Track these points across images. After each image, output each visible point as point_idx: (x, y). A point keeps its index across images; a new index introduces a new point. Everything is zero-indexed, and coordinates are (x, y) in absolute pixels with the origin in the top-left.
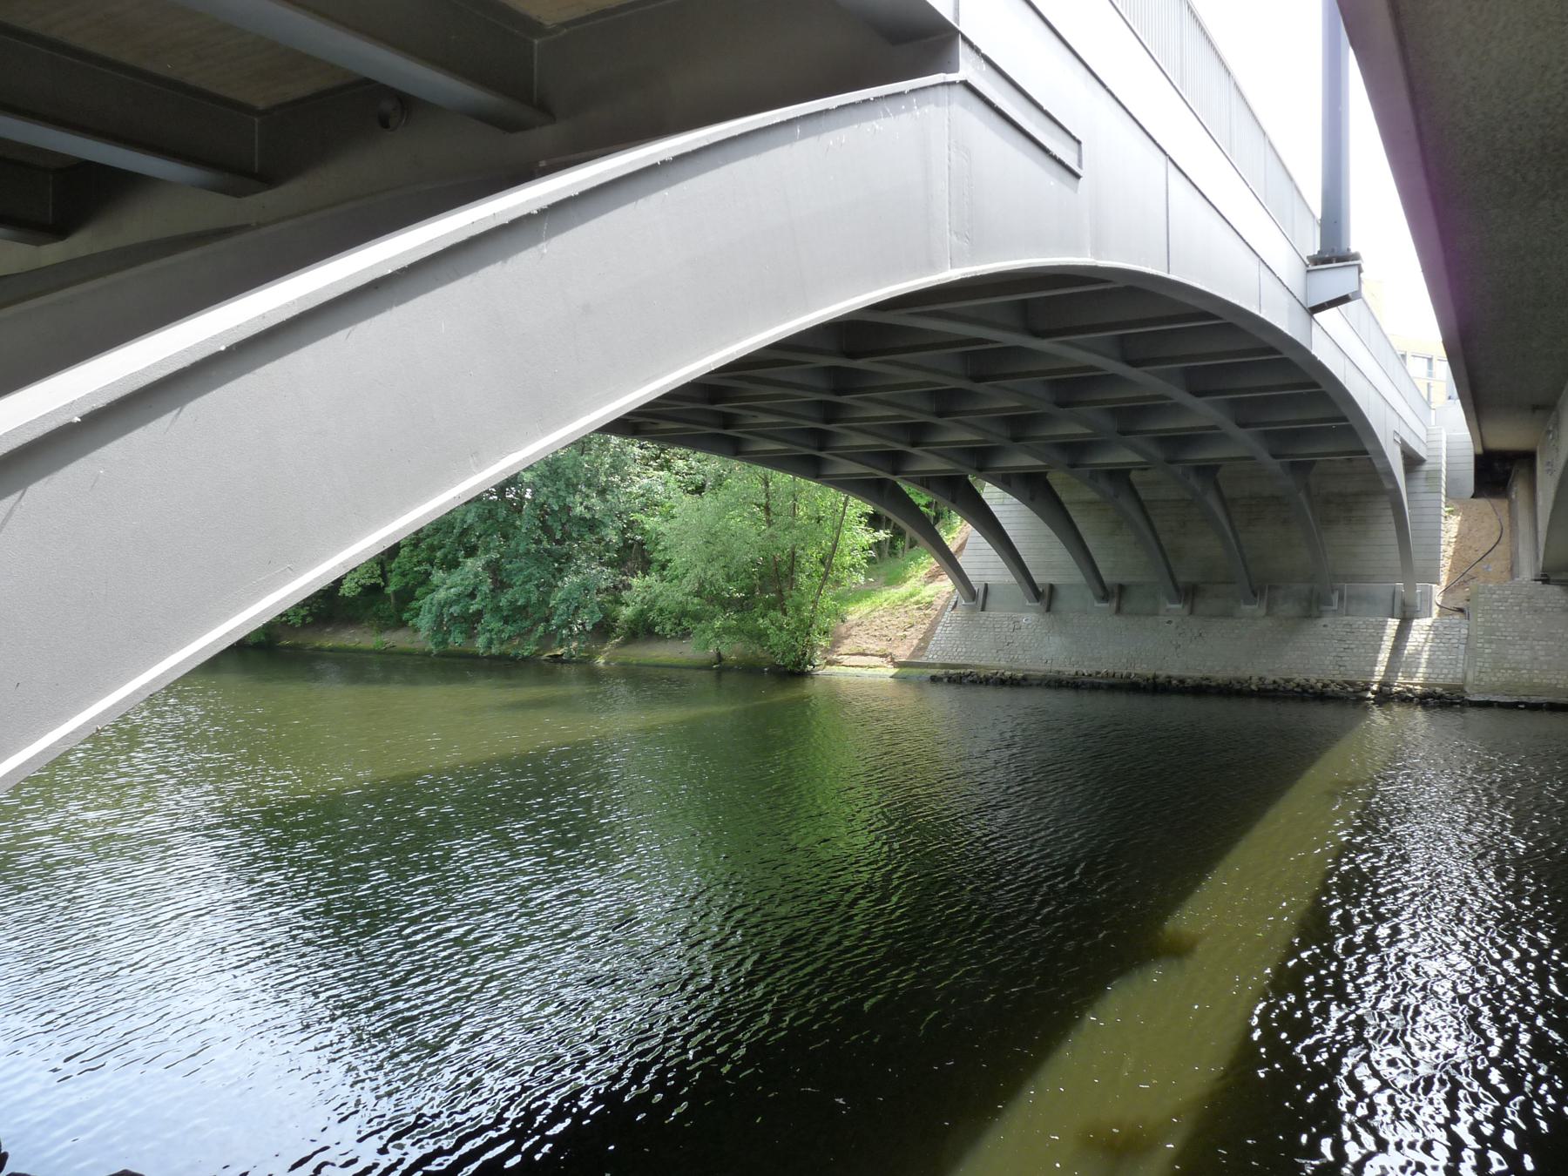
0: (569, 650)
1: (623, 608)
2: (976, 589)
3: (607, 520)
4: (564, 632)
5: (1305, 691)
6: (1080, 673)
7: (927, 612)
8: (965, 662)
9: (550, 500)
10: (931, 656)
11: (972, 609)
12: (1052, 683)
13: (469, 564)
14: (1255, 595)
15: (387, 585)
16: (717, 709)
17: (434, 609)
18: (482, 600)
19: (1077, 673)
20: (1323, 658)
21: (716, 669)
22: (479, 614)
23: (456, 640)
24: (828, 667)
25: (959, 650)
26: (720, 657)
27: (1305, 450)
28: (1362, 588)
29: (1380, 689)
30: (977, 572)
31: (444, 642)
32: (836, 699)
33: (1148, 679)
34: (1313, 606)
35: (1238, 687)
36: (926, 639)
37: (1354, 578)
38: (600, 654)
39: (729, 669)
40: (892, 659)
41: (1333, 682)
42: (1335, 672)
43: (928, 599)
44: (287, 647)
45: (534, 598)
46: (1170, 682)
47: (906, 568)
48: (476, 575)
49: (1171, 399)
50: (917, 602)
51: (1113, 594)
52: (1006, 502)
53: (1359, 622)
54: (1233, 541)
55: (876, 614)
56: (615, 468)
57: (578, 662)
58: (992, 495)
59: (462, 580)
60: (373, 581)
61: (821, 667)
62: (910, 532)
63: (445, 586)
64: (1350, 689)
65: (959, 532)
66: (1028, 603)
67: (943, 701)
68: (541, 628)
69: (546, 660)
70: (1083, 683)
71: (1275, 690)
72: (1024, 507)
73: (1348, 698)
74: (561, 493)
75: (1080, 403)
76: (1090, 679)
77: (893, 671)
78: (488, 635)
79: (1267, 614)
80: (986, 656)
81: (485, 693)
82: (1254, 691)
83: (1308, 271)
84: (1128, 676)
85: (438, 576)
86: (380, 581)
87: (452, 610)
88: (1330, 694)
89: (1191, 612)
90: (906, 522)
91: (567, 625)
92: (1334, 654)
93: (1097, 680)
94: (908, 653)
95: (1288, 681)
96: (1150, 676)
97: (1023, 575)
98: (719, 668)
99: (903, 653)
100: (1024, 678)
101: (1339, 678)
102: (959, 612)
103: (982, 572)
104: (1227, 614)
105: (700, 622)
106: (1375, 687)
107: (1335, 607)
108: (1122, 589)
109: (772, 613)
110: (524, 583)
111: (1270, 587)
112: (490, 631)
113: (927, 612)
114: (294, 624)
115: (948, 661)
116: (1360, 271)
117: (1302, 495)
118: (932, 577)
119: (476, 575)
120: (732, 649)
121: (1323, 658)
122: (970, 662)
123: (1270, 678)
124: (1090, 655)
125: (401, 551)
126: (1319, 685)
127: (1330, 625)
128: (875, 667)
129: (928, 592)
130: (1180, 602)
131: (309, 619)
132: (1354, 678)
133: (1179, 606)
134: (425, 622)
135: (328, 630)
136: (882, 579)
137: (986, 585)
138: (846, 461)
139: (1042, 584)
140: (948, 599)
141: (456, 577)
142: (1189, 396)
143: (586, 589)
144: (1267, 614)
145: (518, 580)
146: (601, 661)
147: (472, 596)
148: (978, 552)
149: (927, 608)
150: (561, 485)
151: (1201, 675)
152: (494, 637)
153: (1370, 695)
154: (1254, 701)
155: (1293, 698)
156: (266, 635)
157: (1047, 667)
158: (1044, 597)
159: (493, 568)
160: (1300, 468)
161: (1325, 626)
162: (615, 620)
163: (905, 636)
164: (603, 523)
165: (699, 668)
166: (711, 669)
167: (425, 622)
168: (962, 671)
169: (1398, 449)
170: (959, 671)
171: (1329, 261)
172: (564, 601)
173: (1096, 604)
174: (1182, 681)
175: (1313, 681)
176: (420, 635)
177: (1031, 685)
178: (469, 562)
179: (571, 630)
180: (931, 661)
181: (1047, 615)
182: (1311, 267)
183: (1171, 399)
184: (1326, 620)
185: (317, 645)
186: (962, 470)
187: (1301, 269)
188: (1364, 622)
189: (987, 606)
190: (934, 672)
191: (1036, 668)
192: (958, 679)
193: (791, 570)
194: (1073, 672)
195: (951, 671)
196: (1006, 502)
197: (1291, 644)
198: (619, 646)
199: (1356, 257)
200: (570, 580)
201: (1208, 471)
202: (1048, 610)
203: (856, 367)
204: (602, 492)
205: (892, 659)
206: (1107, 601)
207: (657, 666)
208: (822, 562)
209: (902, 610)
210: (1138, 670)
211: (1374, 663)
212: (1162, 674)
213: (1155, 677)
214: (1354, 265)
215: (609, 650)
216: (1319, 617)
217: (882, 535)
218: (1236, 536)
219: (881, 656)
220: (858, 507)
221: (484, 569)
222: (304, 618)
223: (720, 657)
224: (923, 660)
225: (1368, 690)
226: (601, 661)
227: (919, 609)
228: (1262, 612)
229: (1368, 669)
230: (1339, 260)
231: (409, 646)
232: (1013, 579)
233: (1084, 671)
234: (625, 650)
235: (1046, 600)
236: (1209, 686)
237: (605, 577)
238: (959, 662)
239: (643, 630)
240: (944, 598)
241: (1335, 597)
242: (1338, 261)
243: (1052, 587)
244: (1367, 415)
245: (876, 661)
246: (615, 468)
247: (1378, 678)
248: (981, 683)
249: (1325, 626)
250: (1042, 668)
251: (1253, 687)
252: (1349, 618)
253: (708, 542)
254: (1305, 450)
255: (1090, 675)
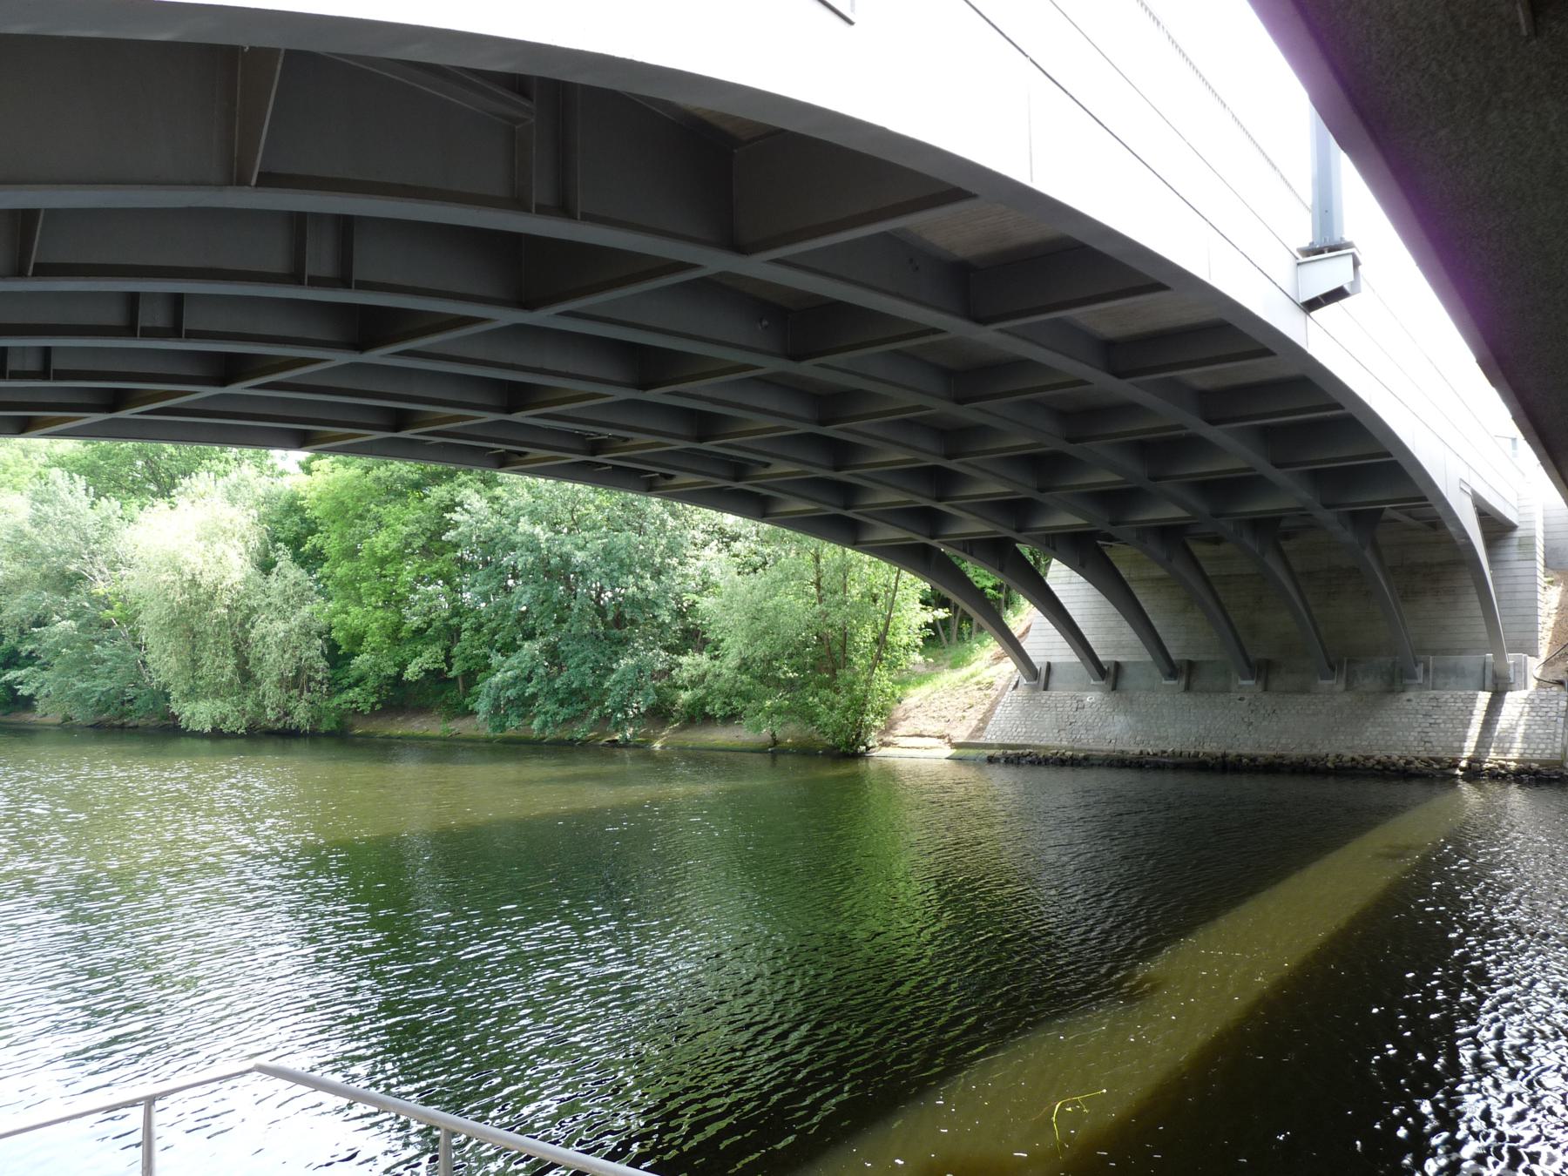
0: (625, 736)
1: (681, 692)
2: (1038, 668)
3: (661, 601)
4: (619, 715)
5: (1386, 768)
6: (1145, 752)
7: (987, 692)
8: (1025, 742)
9: (603, 580)
10: (991, 736)
11: (1034, 689)
12: (1115, 763)
13: (526, 646)
14: (1332, 668)
15: (450, 669)
16: (763, 781)
17: (492, 692)
18: (538, 683)
19: (1141, 752)
20: (1407, 734)
21: (772, 752)
22: (534, 696)
23: (513, 726)
24: (884, 749)
25: (1019, 730)
26: (775, 742)
27: (1364, 498)
28: (1453, 660)
29: (1469, 765)
30: (1043, 653)
31: (502, 727)
32: (889, 774)
33: (1217, 758)
34: (1397, 679)
35: (1313, 764)
36: (984, 720)
37: (1447, 651)
38: (657, 739)
39: (784, 751)
40: (950, 740)
41: (1417, 758)
42: (1420, 749)
43: (989, 680)
44: (359, 735)
45: (589, 682)
46: (1241, 760)
47: (971, 650)
48: (533, 658)
49: (1186, 428)
50: (978, 683)
51: (1182, 672)
52: (1073, 580)
53: (1446, 695)
54: (1305, 615)
55: (935, 695)
56: (672, 550)
57: (637, 746)
58: (1061, 577)
59: (519, 663)
60: (436, 666)
61: (877, 749)
62: (978, 618)
63: (503, 670)
64: (1436, 766)
65: (1025, 617)
66: (1092, 682)
67: (1003, 781)
68: (596, 712)
69: (603, 745)
70: (1147, 763)
71: (1353, 768)
72: (1090, 586)
73: (1434, 776)
74: (615, 574)
75: (1090, 439)
76: (1156, 759)
77: (951, 752)
78: (543, 717)
79: (1347, 690)
80: (1048, 736)
81: (537, 769)
82: (1330, 769)
83: (1299, 264)
84: (1196, 755)
85: (496, 659)
86: (444, 666)
87: (508, 693)
88: (1413, 771)
89: (1265, 689)
90: (971, 605)
91: (622, 708)
92: (1419, 729)
93: (1163, 760)
94: (966, 734)
95: (1367, 758)
96: (1219, 755)
97: (1083, 648)
98: (774, 751)
99: (961, 735)
100: (1086, 758)
101: (1424, 755)
102: (1021, 691)
103: (1049, 653)
104: (1304, 690)
105: (749, 702)
106: (1463, 764)
107: (1420, 681)
108: (1191, 665)
109: (823, 692)
110: (578, 666)
111: (1348, 662)
112: (546, 713)
113: (987, 692)
114: (363, 711)
115: (1007, 742)
116: (1356, 264)
117: (1368, 554)
118: (998, 659)
119: (533, 658)
120: (790, 732)
121: (1407, 734)
122: (1030, 742)
123: (1348, 755)
124: (1156, 734)
125: (462, 636)
126: (1402, 762)
127: (1414, 699)
128: (931, 748)
129: (987, 675)
130: (1253, 679)
131: (378, 707)
132: (1442, 755)
133: (1251, 682)
134: (483, 706)
135: (399, 719)
136: (948, 663)
137: (1049, 664)
138: (884, 525)
139: (1107, 662)
140: (1010, 679)
141: (513, 660)
142: (1203, 423)
143: (640, 670)
144: (1347, 690)
145: (573, 662)
146: (657, 745)
147: (529, 679)
148: (1044, 633)
149: (988, 688)
150: (615, 565)
151: (1273, 753)
152: (549, 719)
153: (1458, 772)
154: (1331, 779)
155: (1374, 776)
156: (338, 723)
157: (1111, 747)
158: (1109, 675)
159: (552, 653)
160: (1365, 520)
161: (1409, 700)
162: (673, 704)
163: (964, 717)
164: (657, 604)
165: (753, 751)
166: (768, 752)
167: (483, 706)
168: (1020, 752)
169: (1468, 503)
170: (1017, 751)
171: (1321, 251)
172: (617, 683)
173: (1164, 682)
174: (1253, 759)
175: (1395, 758)
176: (479, 725)
177: (1092, 765)
178: (526, 645)
179: (626, 714)
180: (989, 742)
181: (1113, 693)
182: (1302, 259)
183: (1186, 428)
184: (1411, 695)
185: (387, 733)
186: (1006, 532)
187: (1289, 262)
188: (1452, 697)
189: (1050, 686)
190: (991, 752)
191: (1100, 747)
192: (1016, 758)
193: (844, 648)
194: (1137, 751)
195: (1009, 752)
196: (1073, 580)
197: (1372, 720)
198: (676, 730)
199: (1349, 245)
200: (625, 662)
201: (1265, 527)
202: (1114, 688)
203: (948, 466)
204: (657, 574)
205: (950, 740)
206: (1175, 679)
207: (712, 749)
208: (877, 641)
209: (962, 691)
210: (1207, 749)
211: (1464, 739)
212: (1233, 752)
213: (1224, 756)
214: (1348, 254)
215: (666, 735)
216: (1403, 691)
217: (942, 614)
218: (1308, 610)
219: (939, 737)
220: (912, 586)
221: (541, 652)
222: (373, 705)
223: (775, 742)
224: (982, 740)
225: (1456, 766)
226: (657, 745)
227: (980, 689)
228: (1341, 687)
229: (1456, 744)
230: (1331, 249)
231: (475, 733)
232: (1076, 659)
233: (1149, 750)
234: (683, 735)
235: (1111, 678)
236: (1281, 764)
237: (660, 659)
238: (1018, 742)
239: (698, 716)
240: (1006, 678)
241: (1420, 670)
242: (1330, 251)
243: (1117, 665)
244: (1412, 450)
245: (934, 742)
246: (672, 550)
247: (1467, 754)
248: (1040, 763)
249: (1409, 700)
250: (1105, 748)
251: (1329, 765)
252: (1435, 692)
253: (754, 618)
254: (1364, 498)
255: (1155, 755)
